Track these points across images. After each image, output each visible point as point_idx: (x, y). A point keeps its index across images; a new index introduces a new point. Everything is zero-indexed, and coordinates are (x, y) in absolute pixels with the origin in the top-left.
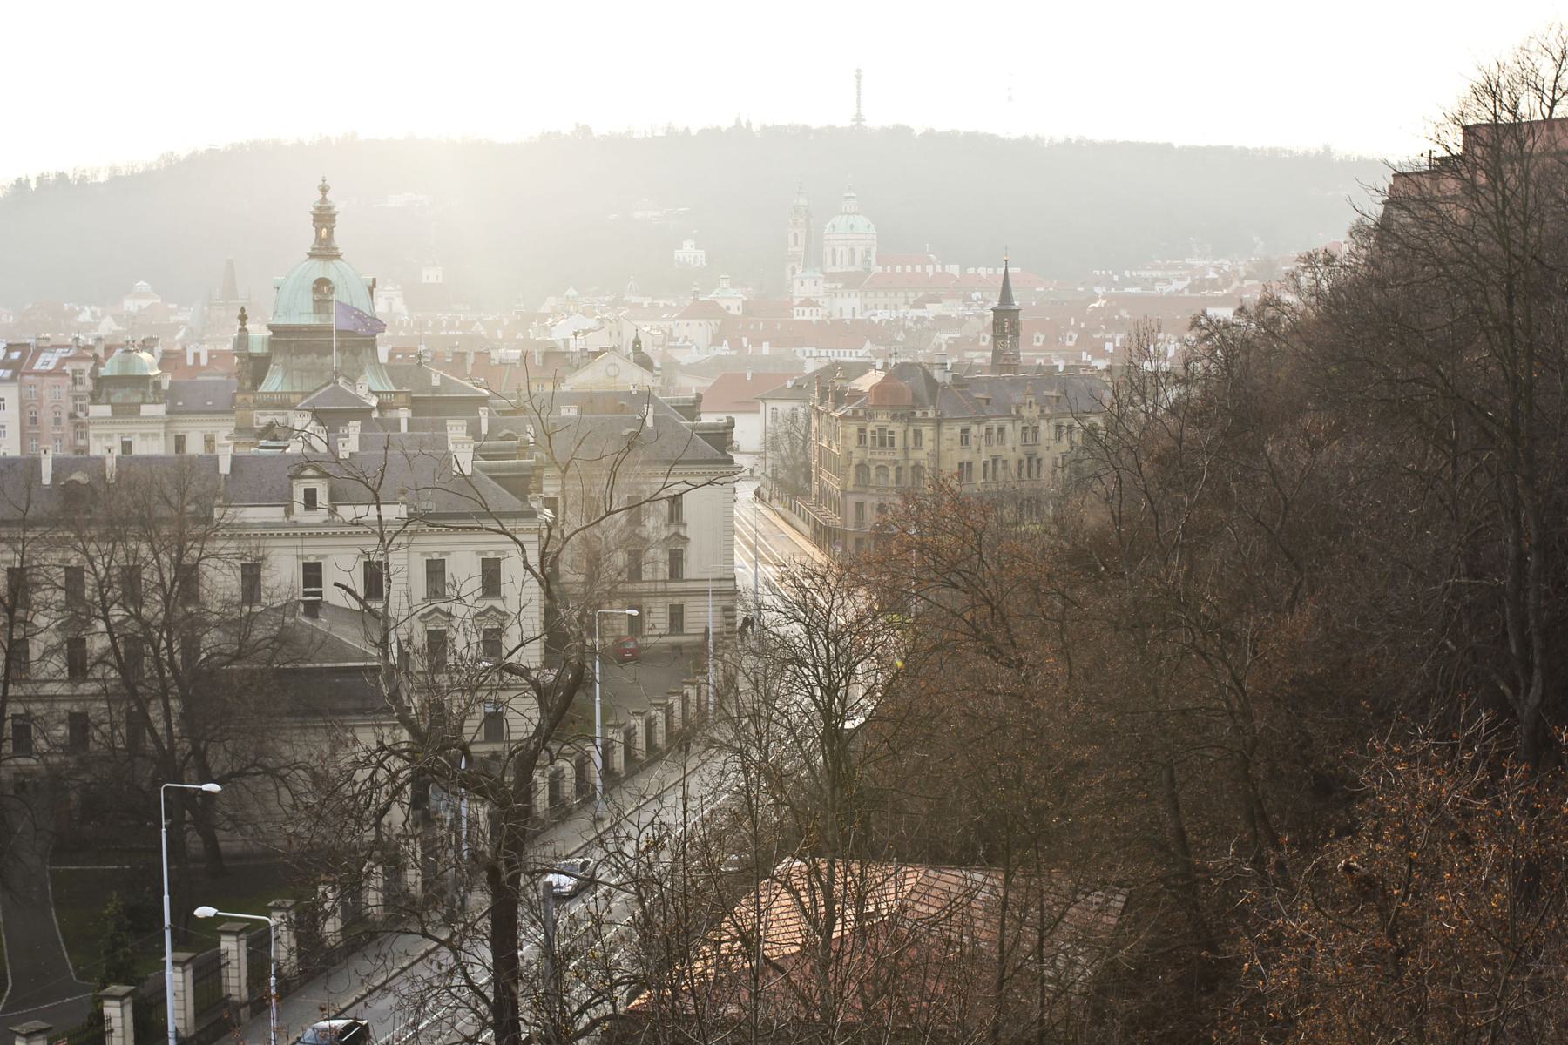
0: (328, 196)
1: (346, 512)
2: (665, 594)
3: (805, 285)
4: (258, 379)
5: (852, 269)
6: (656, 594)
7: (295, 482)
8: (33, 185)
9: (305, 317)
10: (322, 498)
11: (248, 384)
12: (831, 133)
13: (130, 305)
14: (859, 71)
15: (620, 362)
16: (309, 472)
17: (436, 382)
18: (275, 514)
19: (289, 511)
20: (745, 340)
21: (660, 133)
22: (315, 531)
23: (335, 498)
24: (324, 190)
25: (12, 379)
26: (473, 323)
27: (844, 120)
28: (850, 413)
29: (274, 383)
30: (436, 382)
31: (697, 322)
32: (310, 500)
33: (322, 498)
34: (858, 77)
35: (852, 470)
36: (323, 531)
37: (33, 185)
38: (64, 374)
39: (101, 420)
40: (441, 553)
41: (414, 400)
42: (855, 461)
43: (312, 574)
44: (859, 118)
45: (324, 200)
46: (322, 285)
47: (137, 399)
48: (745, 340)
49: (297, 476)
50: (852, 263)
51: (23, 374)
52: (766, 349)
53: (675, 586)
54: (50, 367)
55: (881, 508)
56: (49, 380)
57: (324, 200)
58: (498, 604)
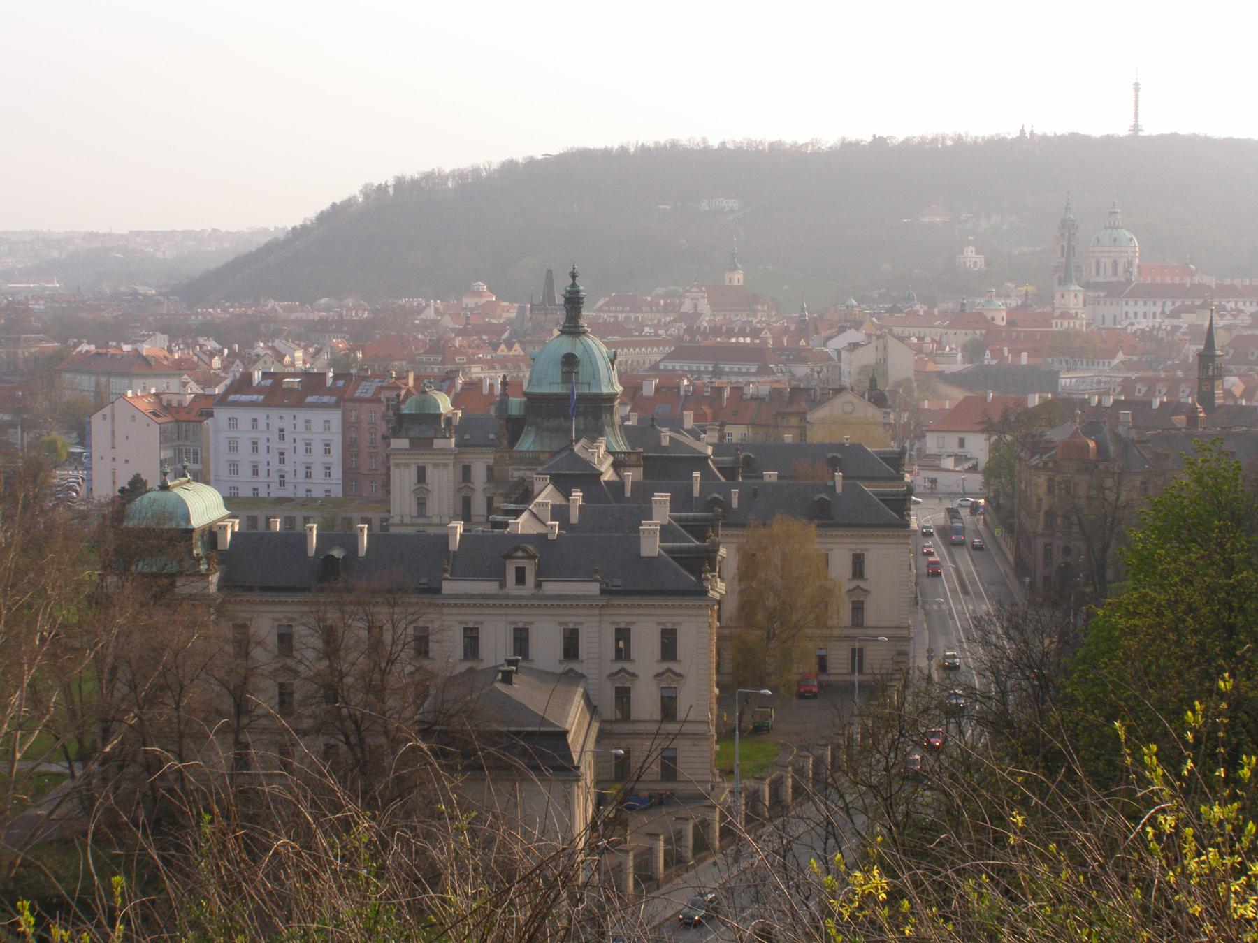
0: (578, 281)
1: (550, 588)
4: (514, 438)
5: (1114, 279)
6: (840, 639)
7: (508, 562)
8: (391, 192)
9: (552, 386)
10: (530, 578)
11: (505, 442)
12: (1108, 141)
13: (469, 302)
14: (1137, 84)
15: (856, 401)
16: (520, 554)
17: (665, 442)
18: (490, 587)
19: (503, 585)
20: (1006, 349)
21: (949, 143)
22: (523, 602)
24: (574, 276)
25: (336, 405)
26: (762, 330)
28: (1041, 465)
29: (527, 443)
30: (665, 442)
31: (964, 331)
33: (530, 578)
35: (1042, 514)
36: (530, 602)
37: (391, 192)
38: (379, 401)
39: (399, 451)
40: (627, 623)
41: (645, 458)
42: (1045, 507)
43: (521, 640)
44: (1136, 128)
45: (574, 285)
47: (431, 434)
48: (1006, 349)
49: (509, 556)
50: (1115, 273)
51: (345, 401)
52: (1024, 358)
54: (368, 396)
55: (1066, 551)
56: (367, 406)
57: (574, 285)
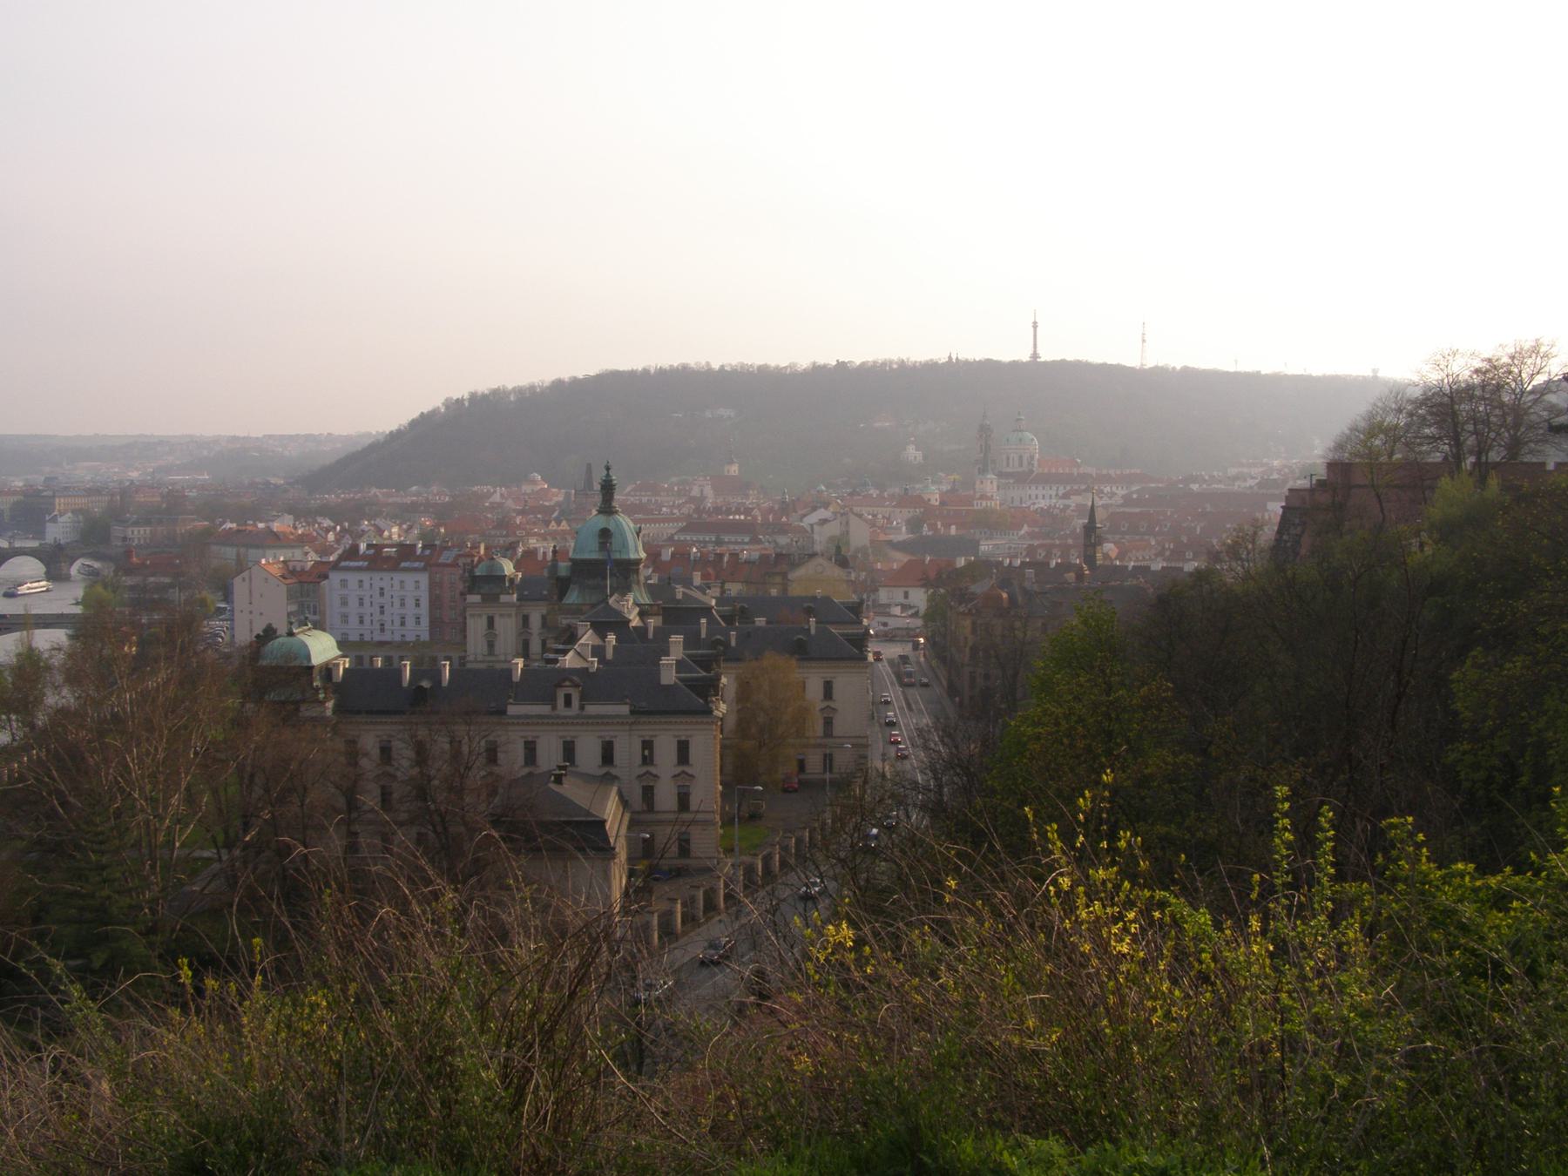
1: (592, 709)
2: (819, 746)
3: (989, 485)
4: (562, 594)
9: (593, 554)
12: (1015, 365)
13: (527, 488)
17: (679, 596)
18: (545, 709)
19: (554, 708)
23: (584, 698)
24: (608, 469)
25: (424, 569)
27: (1025, 357)
29: (573, 597)
32: (568, 702)
34: (1035, 325)
39: (474, 605)
43: (569, 750)
44: (1035, 355)
46: (605, 534)
50: (1021, 465)
53: (829, 741)
58: (686, 769)
